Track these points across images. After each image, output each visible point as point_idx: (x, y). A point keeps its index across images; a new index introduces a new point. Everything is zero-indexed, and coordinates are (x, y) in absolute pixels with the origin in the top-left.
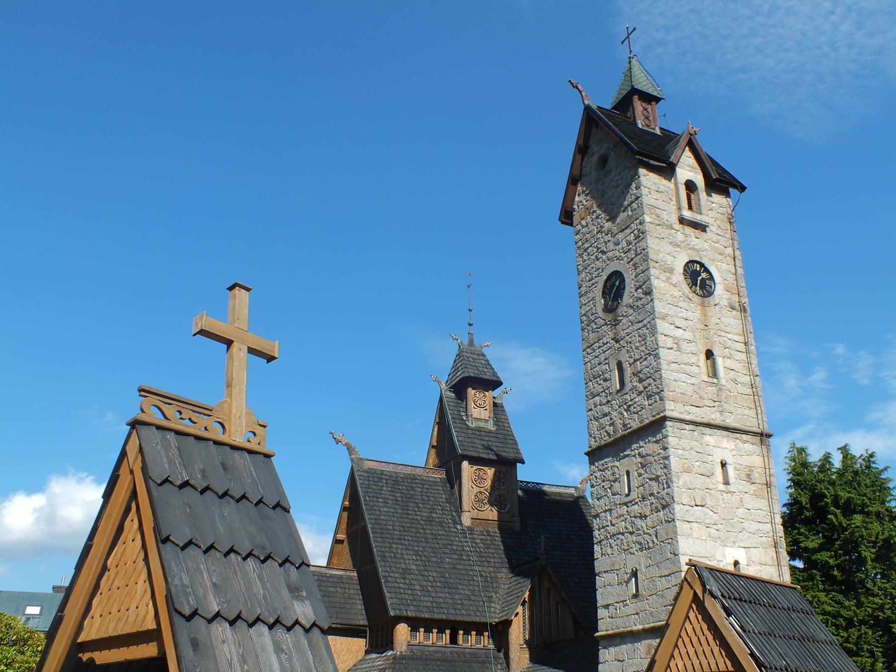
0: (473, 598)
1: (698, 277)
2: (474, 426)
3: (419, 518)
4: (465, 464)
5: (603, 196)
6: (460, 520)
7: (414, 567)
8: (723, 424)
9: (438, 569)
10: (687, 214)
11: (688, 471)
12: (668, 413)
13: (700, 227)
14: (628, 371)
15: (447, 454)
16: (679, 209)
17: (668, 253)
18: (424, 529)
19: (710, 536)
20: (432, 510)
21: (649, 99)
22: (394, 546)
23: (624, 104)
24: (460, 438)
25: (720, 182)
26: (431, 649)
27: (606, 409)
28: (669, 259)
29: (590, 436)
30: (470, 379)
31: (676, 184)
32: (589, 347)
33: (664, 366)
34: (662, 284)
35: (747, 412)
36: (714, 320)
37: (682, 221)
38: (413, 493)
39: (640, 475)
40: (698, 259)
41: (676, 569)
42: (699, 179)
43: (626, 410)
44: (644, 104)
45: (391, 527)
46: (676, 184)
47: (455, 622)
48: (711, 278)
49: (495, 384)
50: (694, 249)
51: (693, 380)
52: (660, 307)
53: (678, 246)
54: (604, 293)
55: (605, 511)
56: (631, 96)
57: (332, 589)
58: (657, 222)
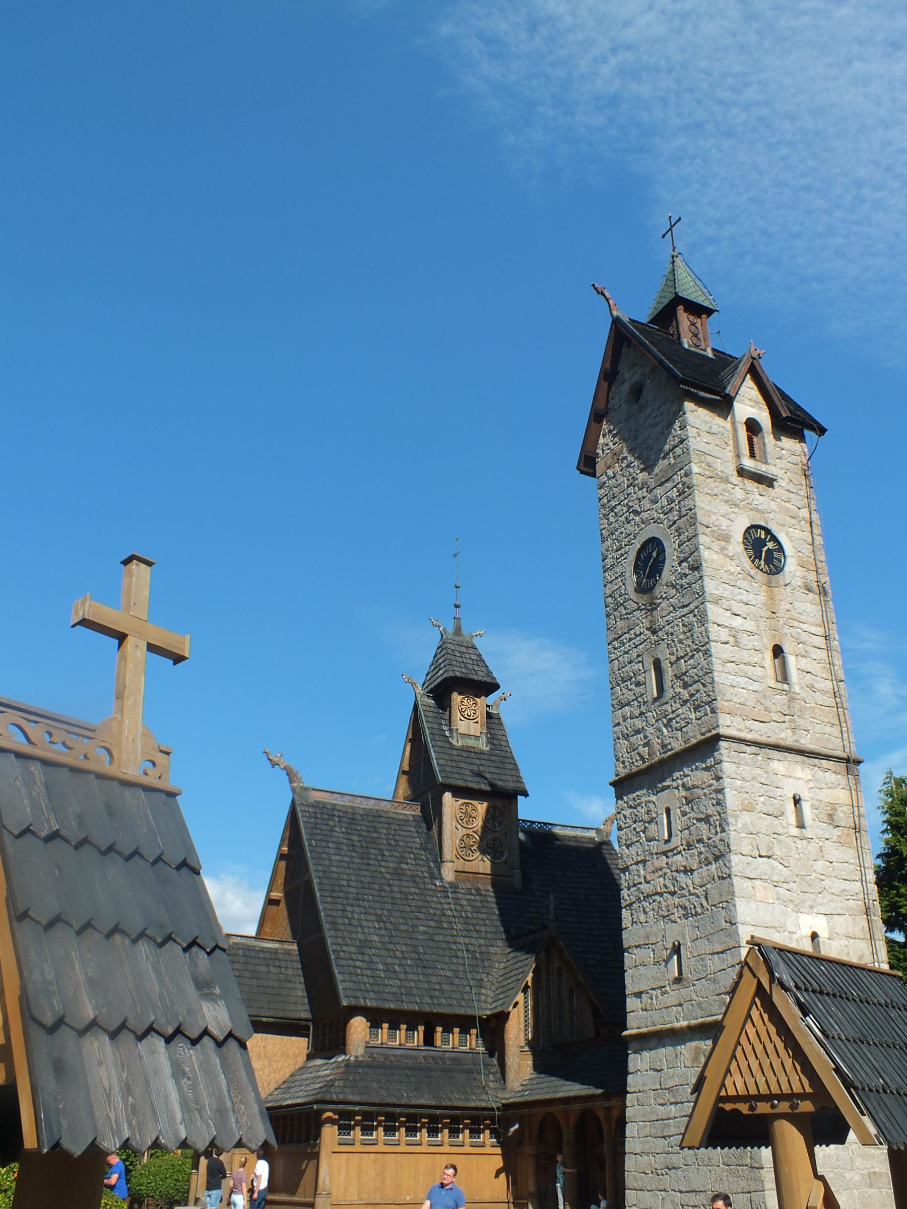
0: (456, 981)
1: (763, 548)
2: (460, 744)
3: (383, 870)
4: (447, 796)
5: (636, 438)
6: (440, 873)
7: (376, 938)
8: (796, 745)
9: (408, 941)
10: (748, 463)
11: (749, 809)
12: (722, 731)
13: (767, 481)
14: (669, 673)
15: (423, 782)
16: (738, 456)
17: (723, 512)
18: (390, 885)
19: (778, 899)
20: (402, 860)
21: (698, 310)
22: (349, 908)
23: (666, 316)
24: (441, 762)
25: (792, 422)
26: (398, 1052)
27: (639, 723)
28: (725, 523)
29: (618, 760)
30: (459, 681)
31: (733, 424)
32: (616, 639)
33: (717, 666)
34: (715, 557)
35: (828, 729)
36: (784, 606)
37: (742, 472)
38: (375, 835)
39: (684, 814)
40: (763, 524)
41: (732, 944)
42: (764, 418)
43: (665, 726)
44: (692, 318)
45: (345, 883)
46: (733, 424)
47: (431, 1014)
48: (781, 549)
49: (488, 687)
50: (757, 510)
51: (756, 686)
52: (711, 587)
53: (736, 505)
54: (636, 567)
55: (637, 863)
56: (674, 306)
57: (263, 968)
58: (708, 473)
